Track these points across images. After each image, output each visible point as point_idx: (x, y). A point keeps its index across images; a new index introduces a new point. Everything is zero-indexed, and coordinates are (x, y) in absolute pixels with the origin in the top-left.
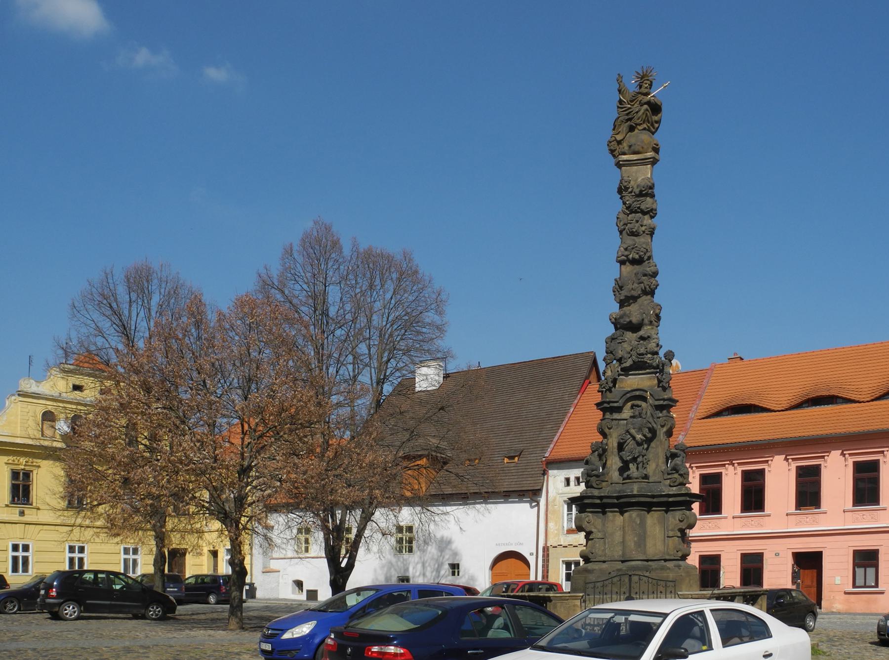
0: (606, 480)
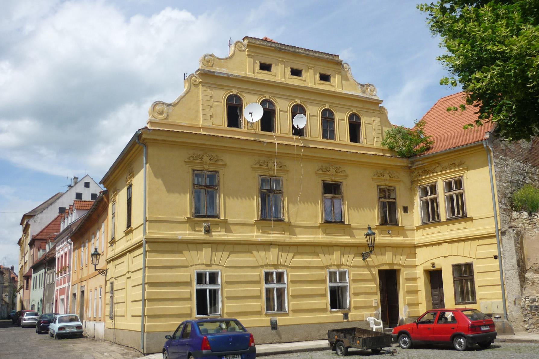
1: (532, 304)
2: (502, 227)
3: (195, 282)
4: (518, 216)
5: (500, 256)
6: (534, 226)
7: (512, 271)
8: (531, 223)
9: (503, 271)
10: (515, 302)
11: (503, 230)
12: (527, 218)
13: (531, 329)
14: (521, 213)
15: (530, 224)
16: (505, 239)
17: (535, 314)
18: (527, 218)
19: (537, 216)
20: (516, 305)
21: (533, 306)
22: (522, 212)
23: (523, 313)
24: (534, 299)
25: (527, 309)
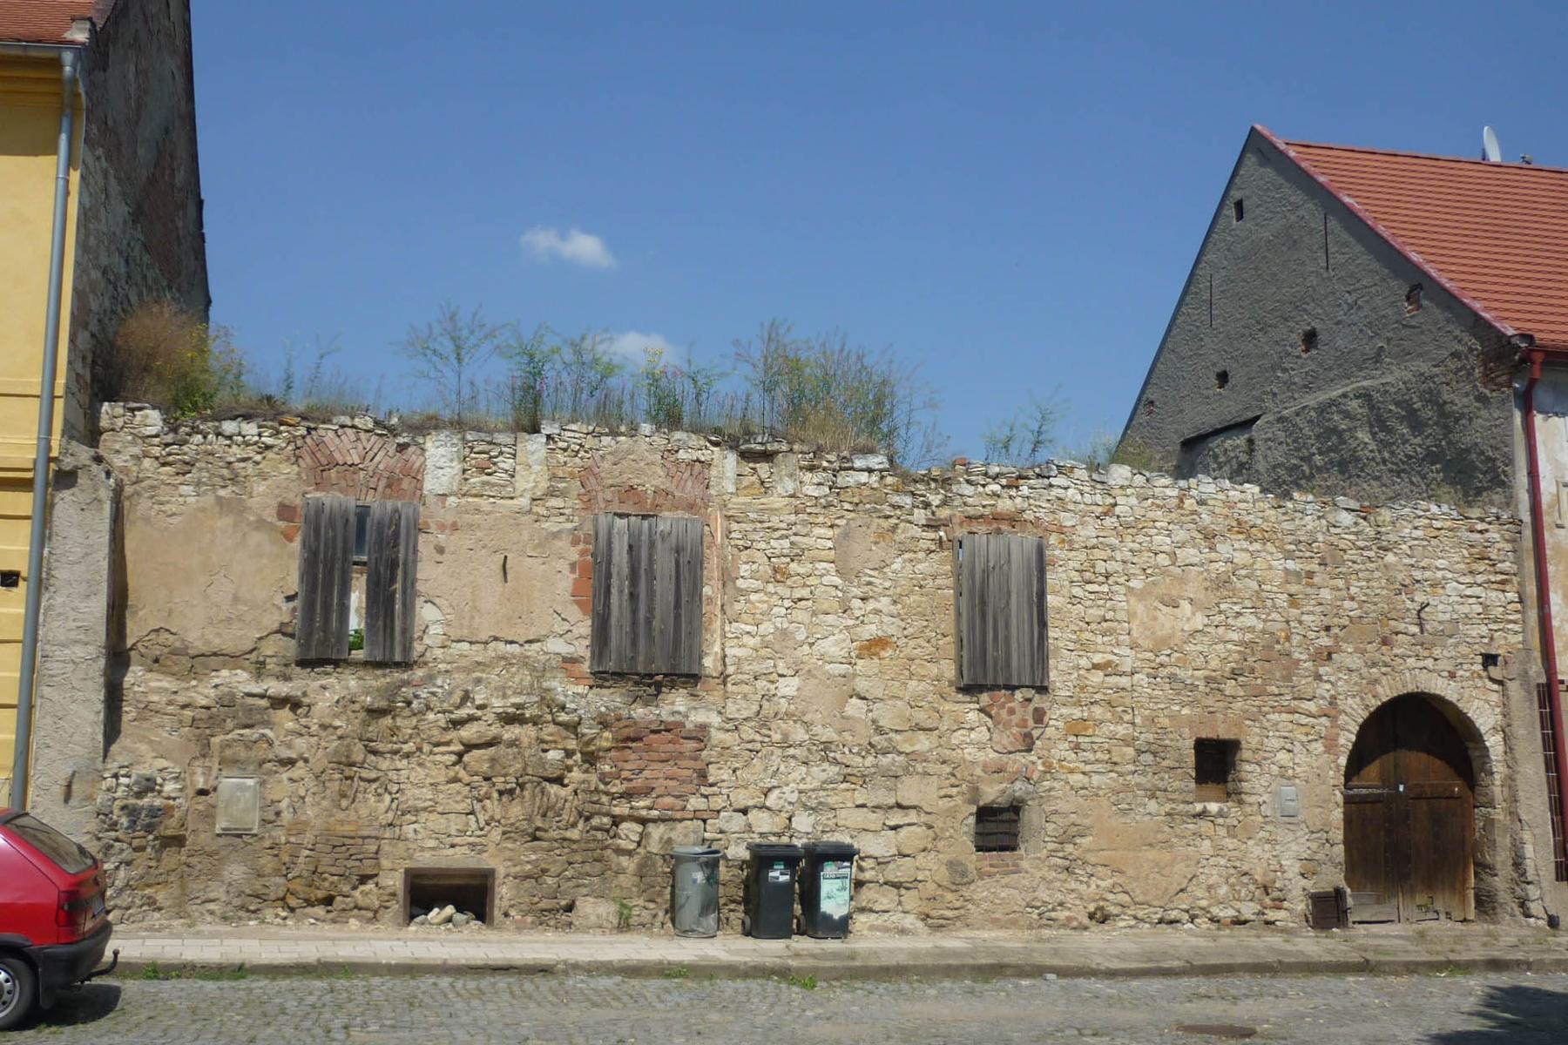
1: (140, 803)
2: (65, 451)
4: (120, 422)
5: (33, 580)
6: (184, 474)
7: (79, 652)
8: (171, 458)
9: (39, 644)
10: (69, 786)
11: (68, 463)
12: (157, 436)
13: (120, 908)
14: (132, 410)
15: (164, 465)
16: (65, 501)
17: (143, 843)
18: (157, 436)
19: (205, 437)
20: (73, 802)
21: (142, 808)
22: (140, 409)
23: (99, 839)
24: (148, 780)
25: (115, 824)
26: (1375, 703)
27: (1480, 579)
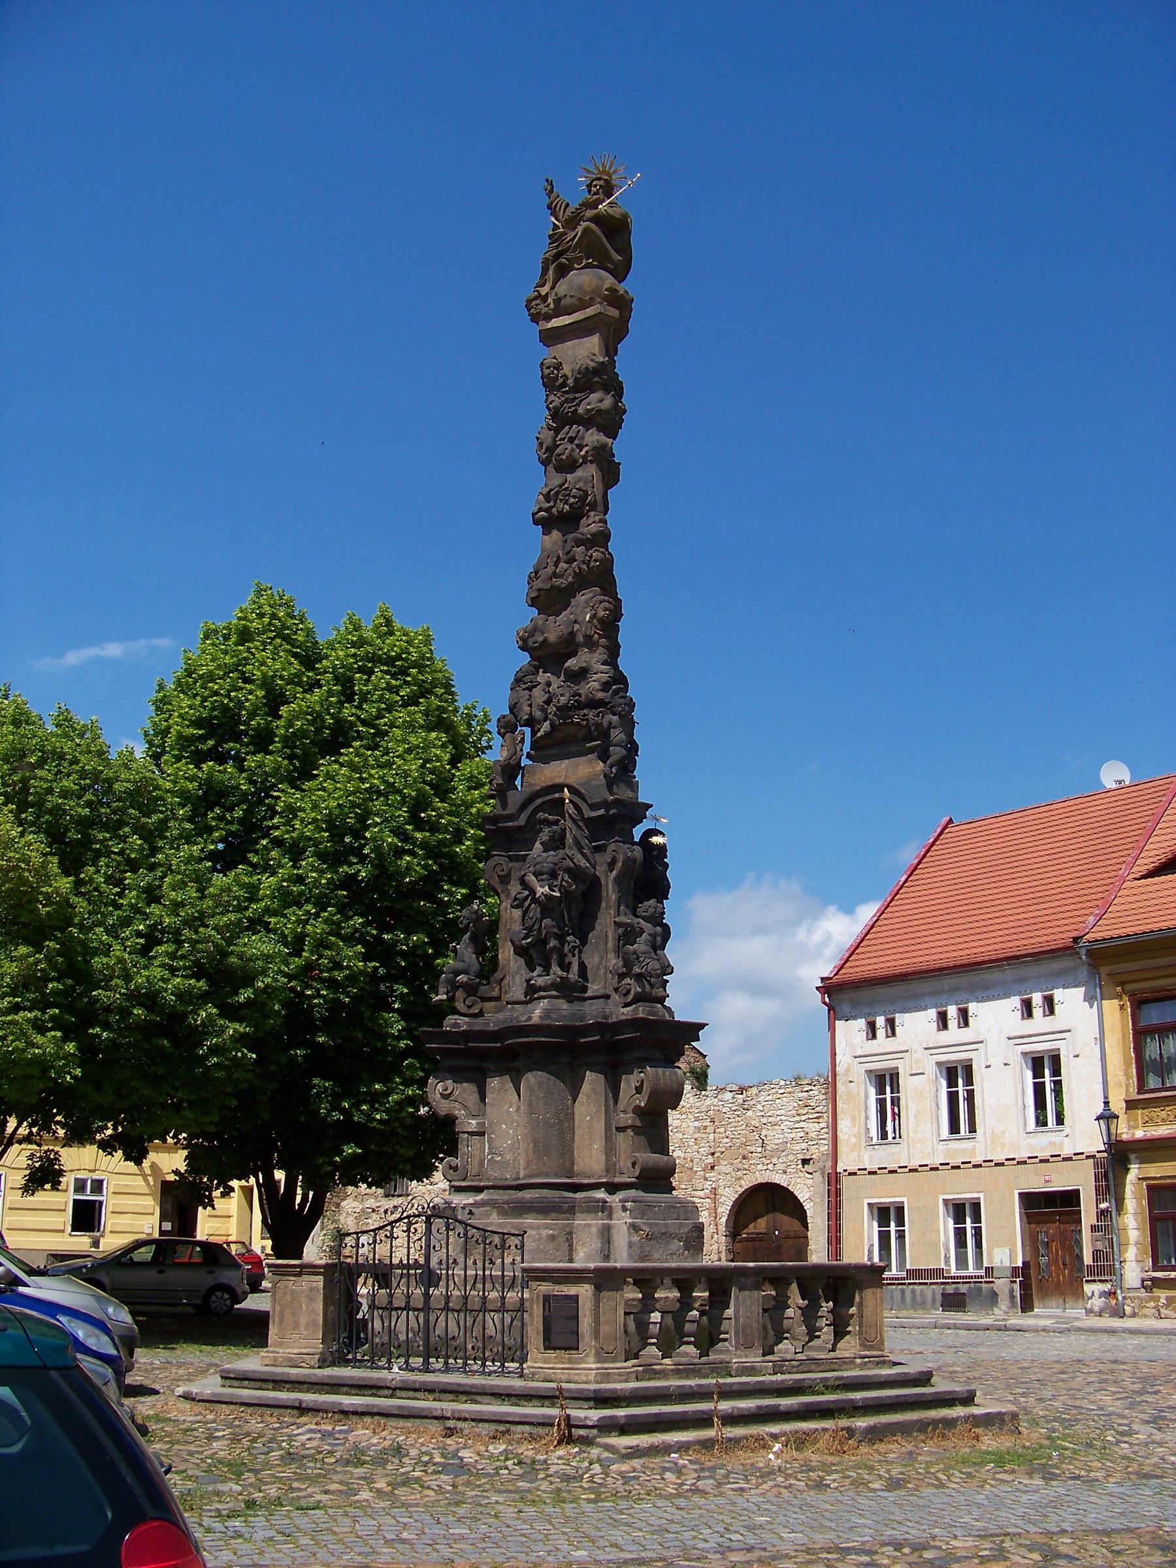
0: (495, 994)
3: (72, 1189)
26: (741, 1190)
27: (803, 1118)
